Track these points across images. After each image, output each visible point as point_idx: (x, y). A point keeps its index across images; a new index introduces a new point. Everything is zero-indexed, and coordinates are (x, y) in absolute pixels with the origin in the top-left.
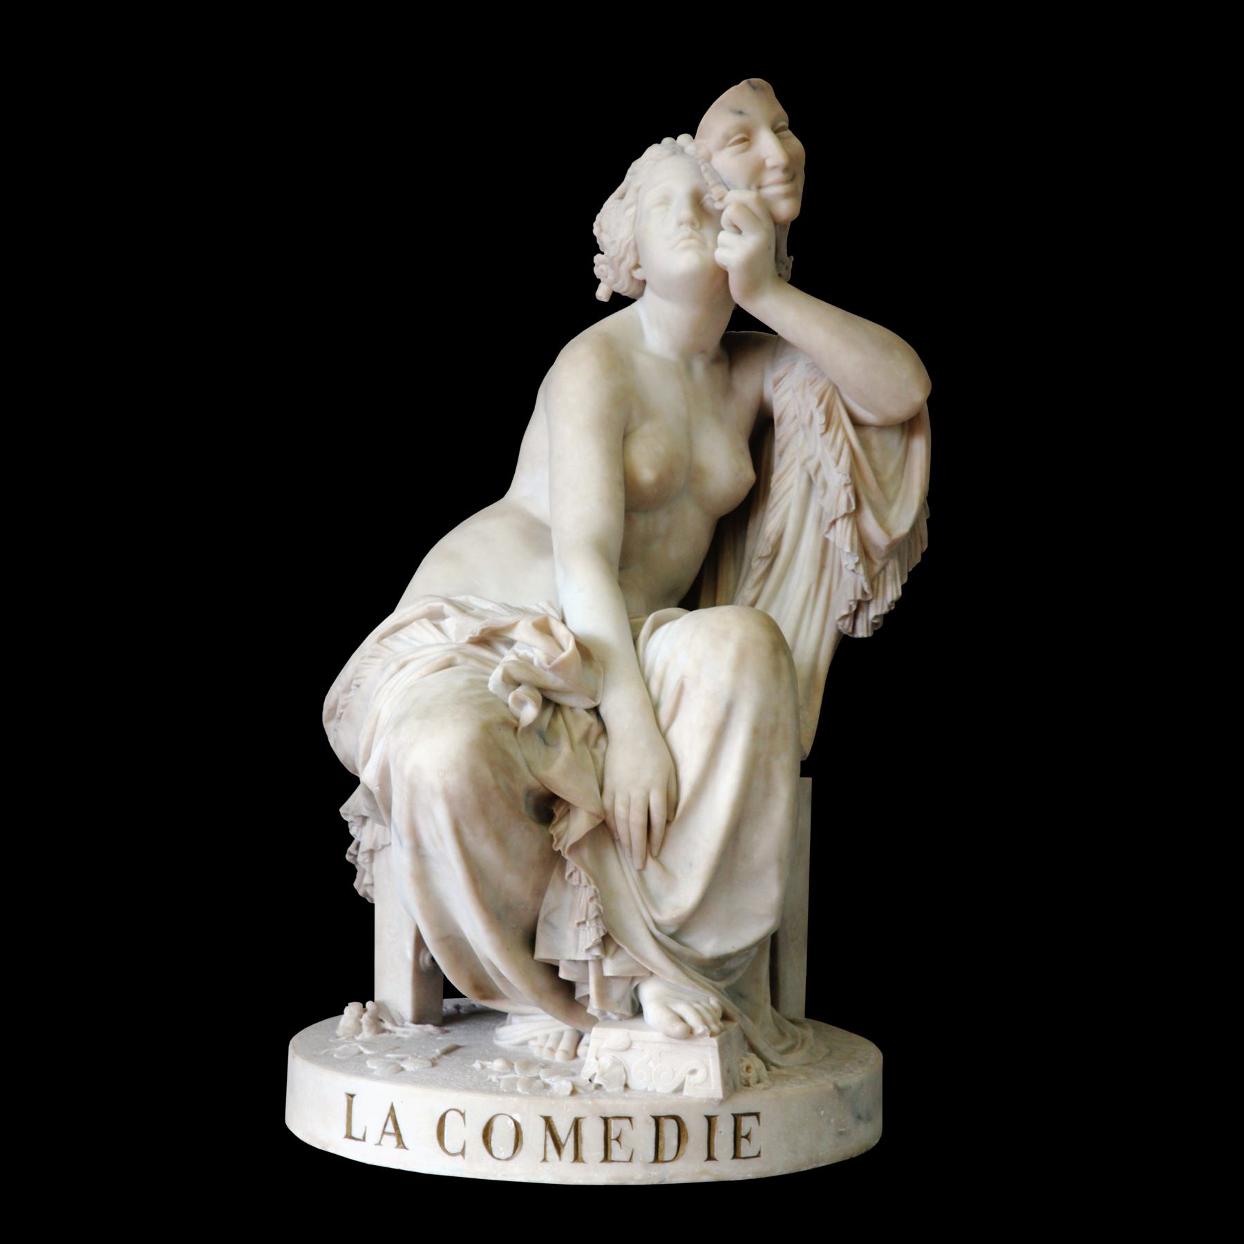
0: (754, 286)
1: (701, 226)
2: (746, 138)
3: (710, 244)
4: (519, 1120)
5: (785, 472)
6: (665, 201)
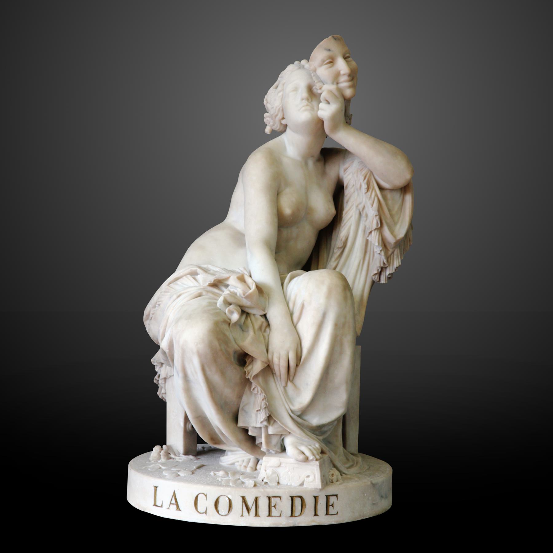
0: (335, 127)
1: (312, 101)
2: (332, 61)
3: (315, 108)
4: (231, 498)
5: (349, 210)
6: (296, 89)
